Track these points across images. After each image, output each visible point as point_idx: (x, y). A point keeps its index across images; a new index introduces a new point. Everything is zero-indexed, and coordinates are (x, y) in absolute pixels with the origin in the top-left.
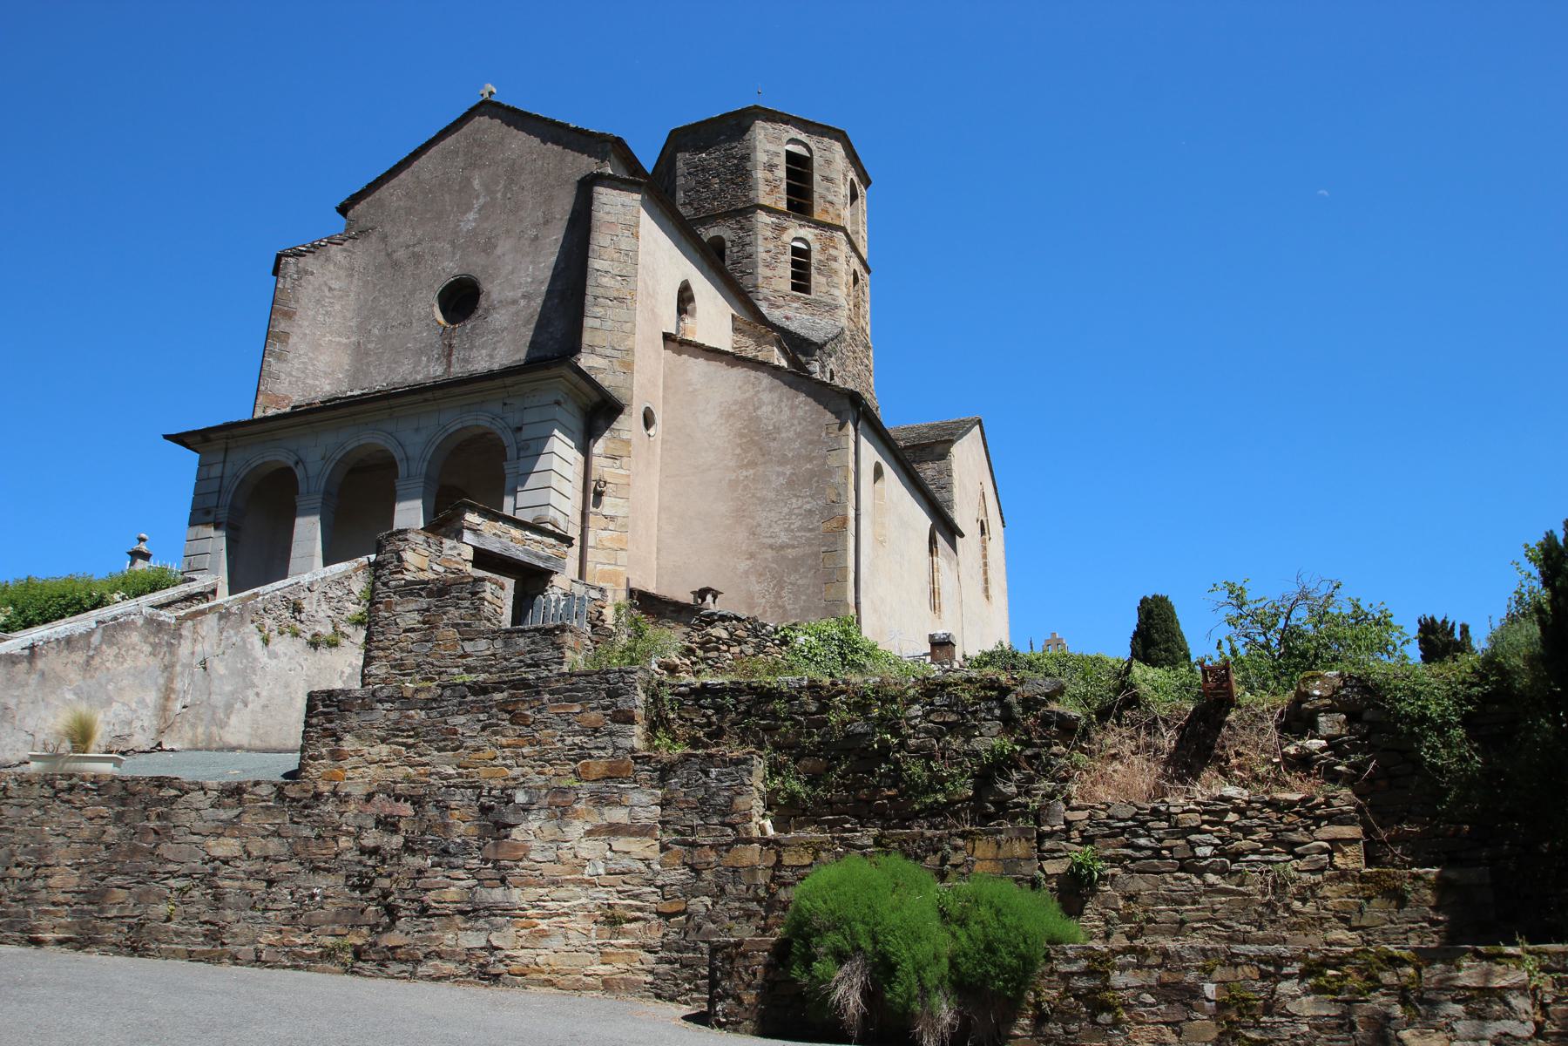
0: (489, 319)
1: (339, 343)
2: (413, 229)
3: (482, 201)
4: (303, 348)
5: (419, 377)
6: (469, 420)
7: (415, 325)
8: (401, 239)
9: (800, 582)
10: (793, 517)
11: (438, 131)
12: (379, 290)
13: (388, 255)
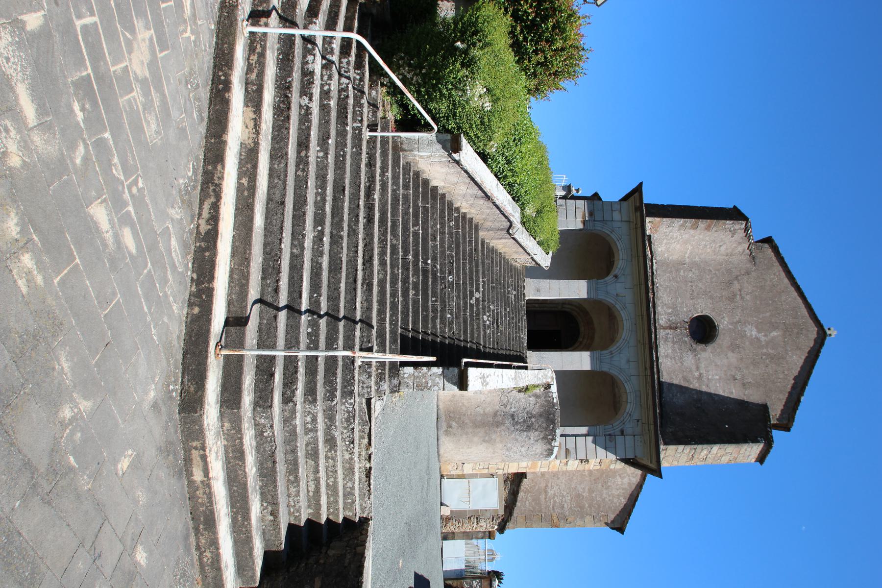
0: (689, 353)
1: (687, 253)
2: (751, 293)
3: (763, 339)
4: (685, 237)
5: (659, 309)
6: (631, 398)
7: (691, 301)
8: (746, 285)
9: (527, 502)
10: (561, 498)
11: (811, 303)
12: (715, 274)
13: (737, 278)
